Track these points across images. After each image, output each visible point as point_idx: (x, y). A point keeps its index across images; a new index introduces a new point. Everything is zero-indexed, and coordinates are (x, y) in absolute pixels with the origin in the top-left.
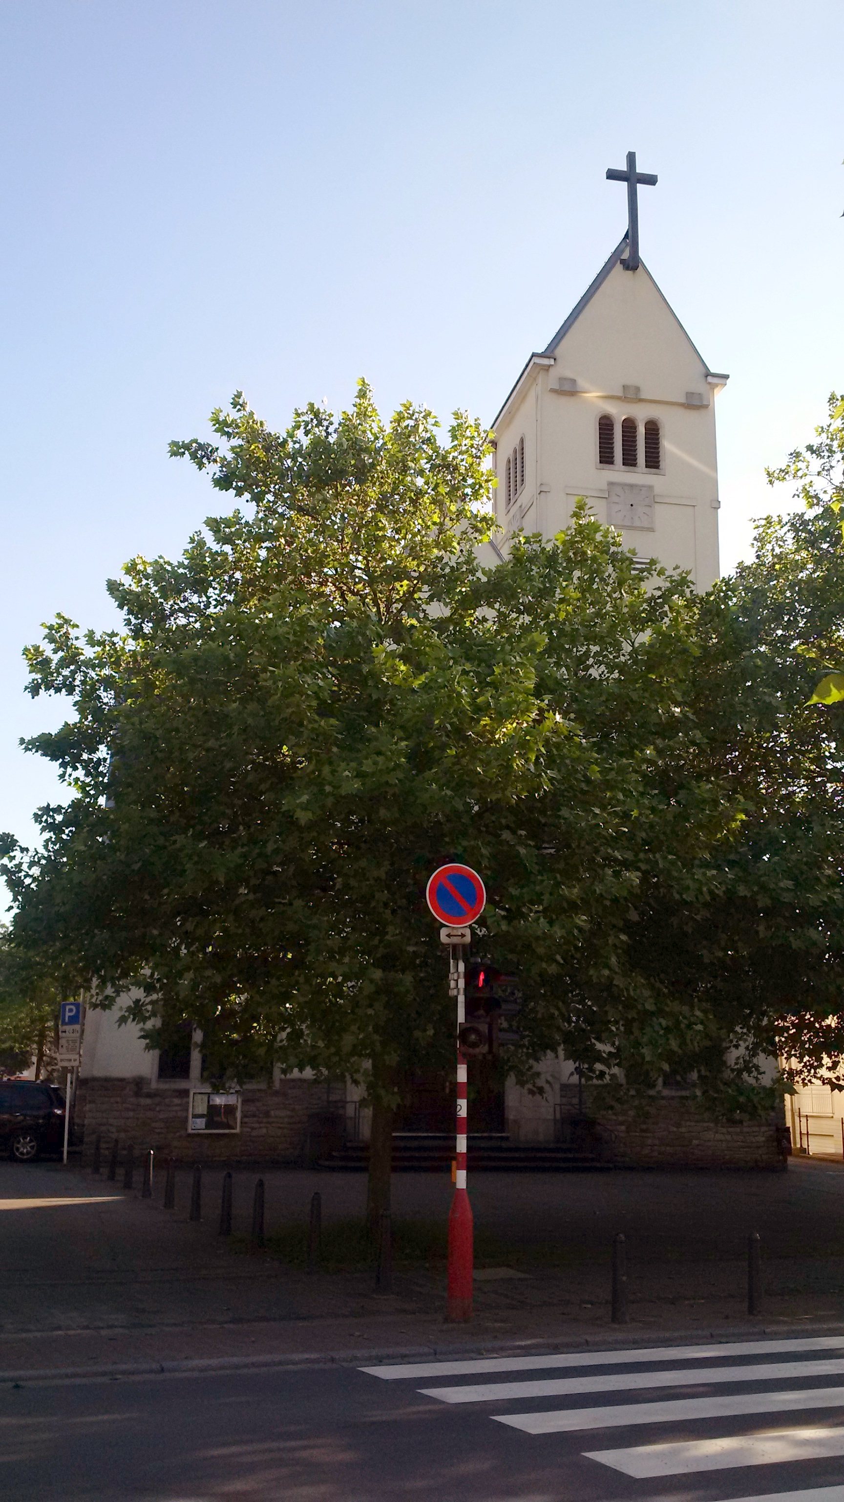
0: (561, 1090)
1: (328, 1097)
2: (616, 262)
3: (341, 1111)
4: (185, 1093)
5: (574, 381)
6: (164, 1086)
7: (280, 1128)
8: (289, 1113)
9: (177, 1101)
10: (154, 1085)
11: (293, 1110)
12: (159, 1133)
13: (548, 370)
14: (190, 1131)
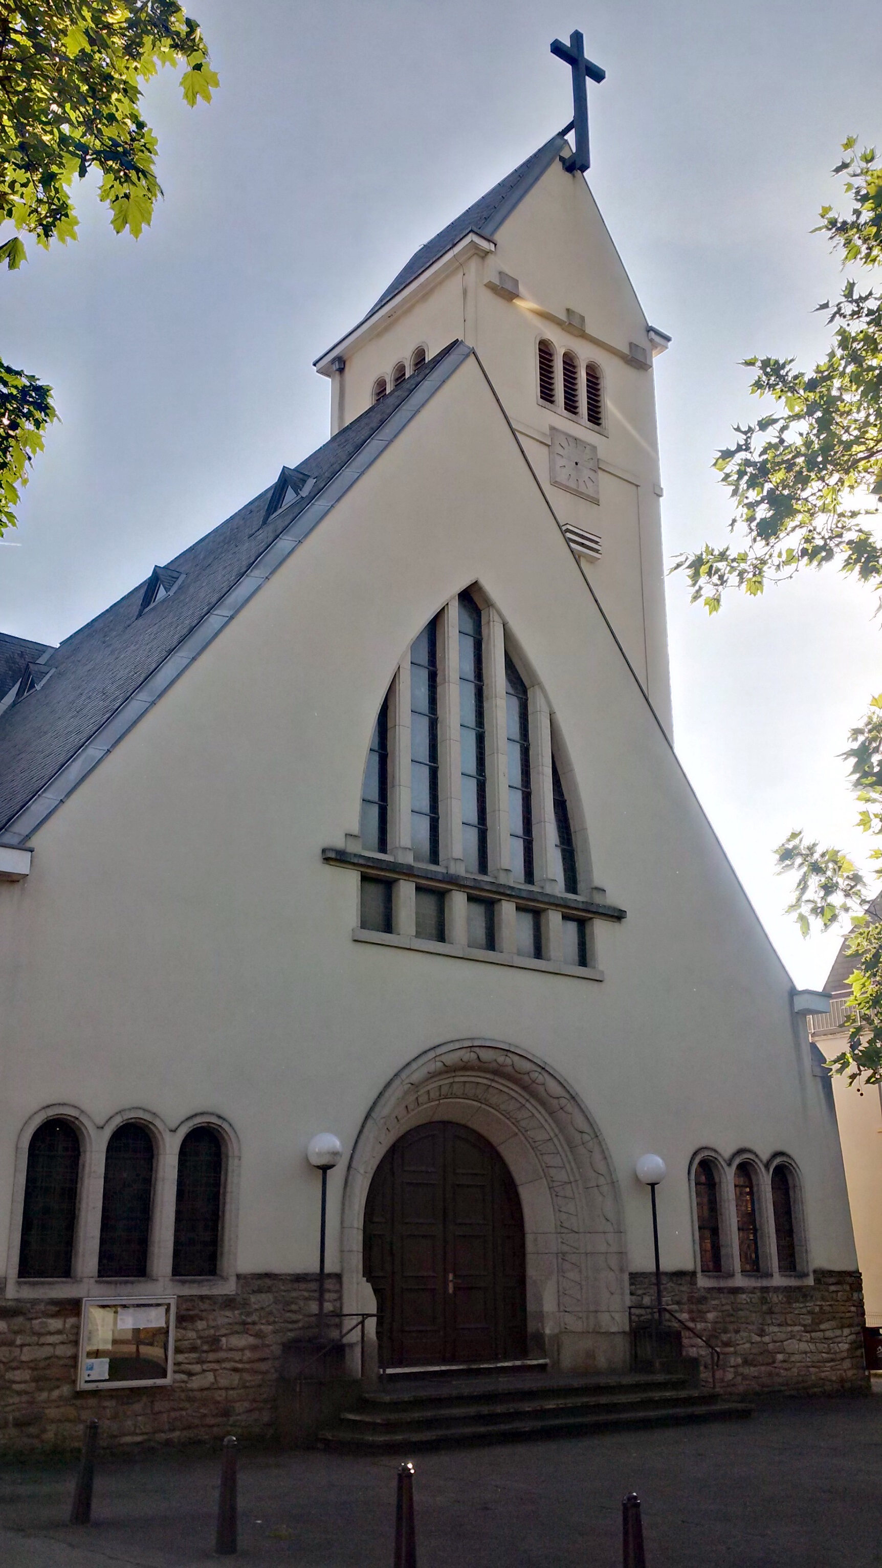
0: (630, 1279)
1: (321, 1306)
2: (552, 160)
3: (334, 1334)
4: (73, 1307)
5: (516, 282)
6: (28, 1293)
7: (235, 1370)
8: (251, 1340)
9: (55, 1324)
10: (11, 1292)
11: (259, 1335)
12: (19, 1393)
13: (483, 258)
14: (82, 1386)
